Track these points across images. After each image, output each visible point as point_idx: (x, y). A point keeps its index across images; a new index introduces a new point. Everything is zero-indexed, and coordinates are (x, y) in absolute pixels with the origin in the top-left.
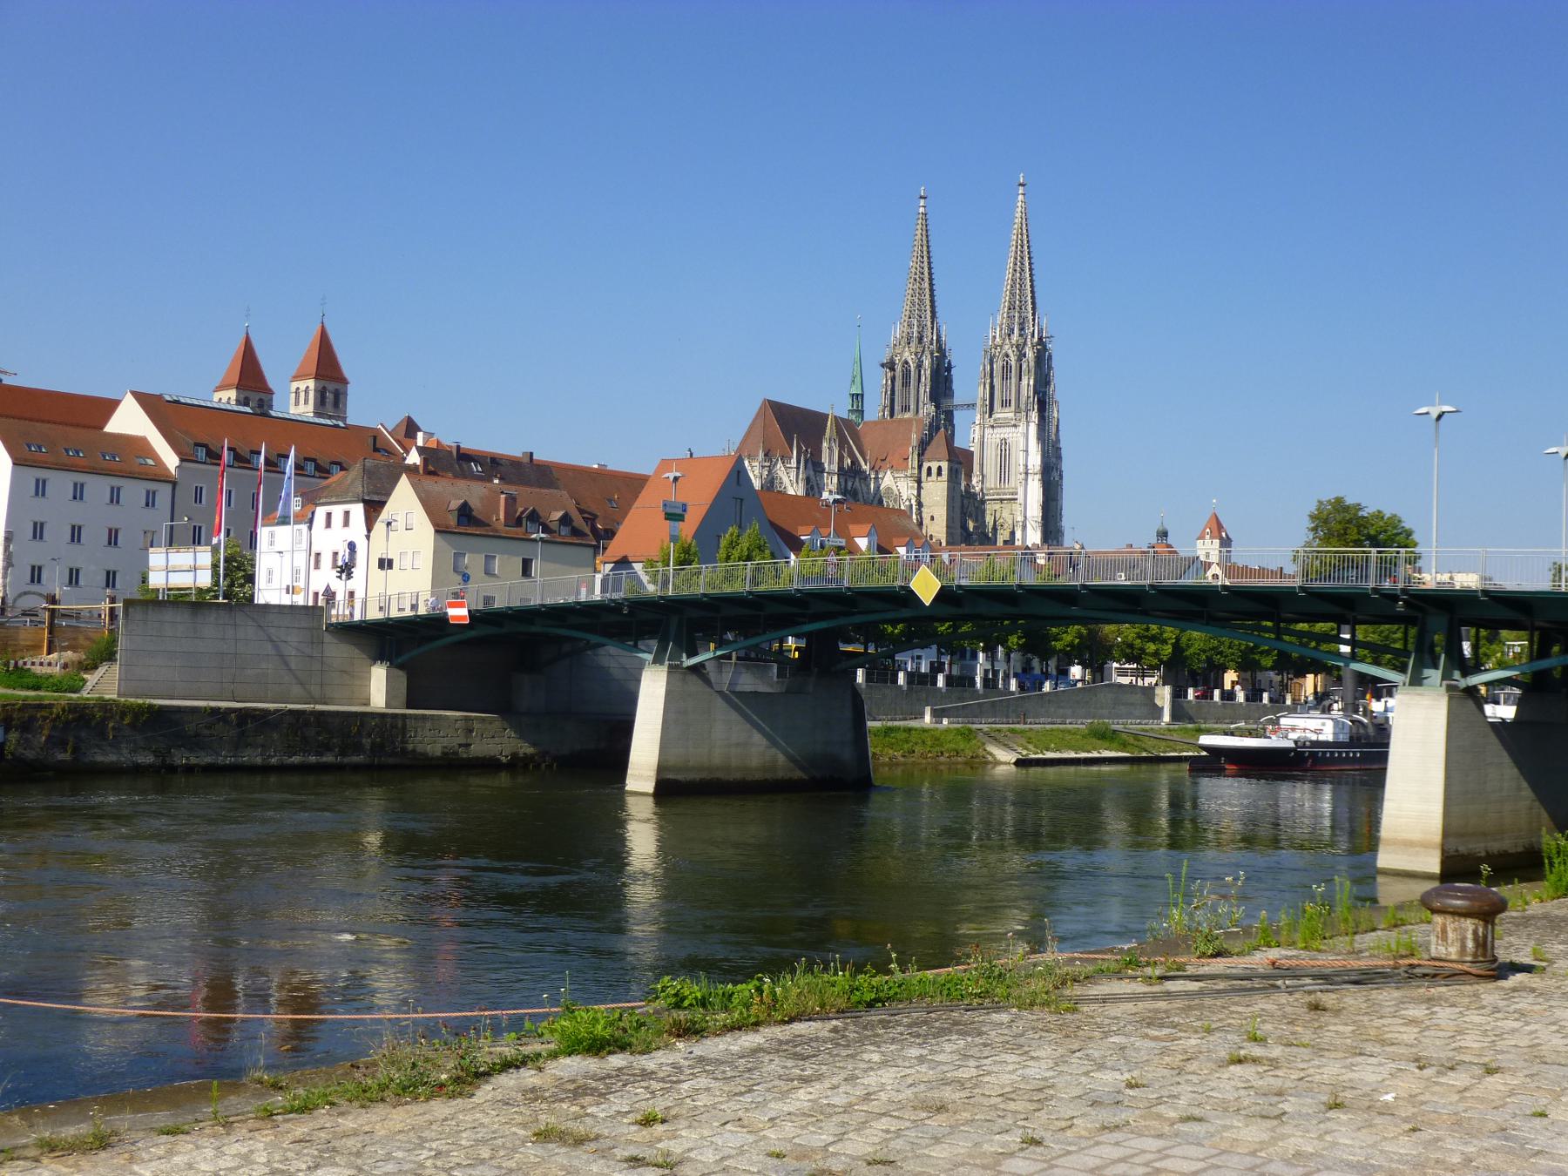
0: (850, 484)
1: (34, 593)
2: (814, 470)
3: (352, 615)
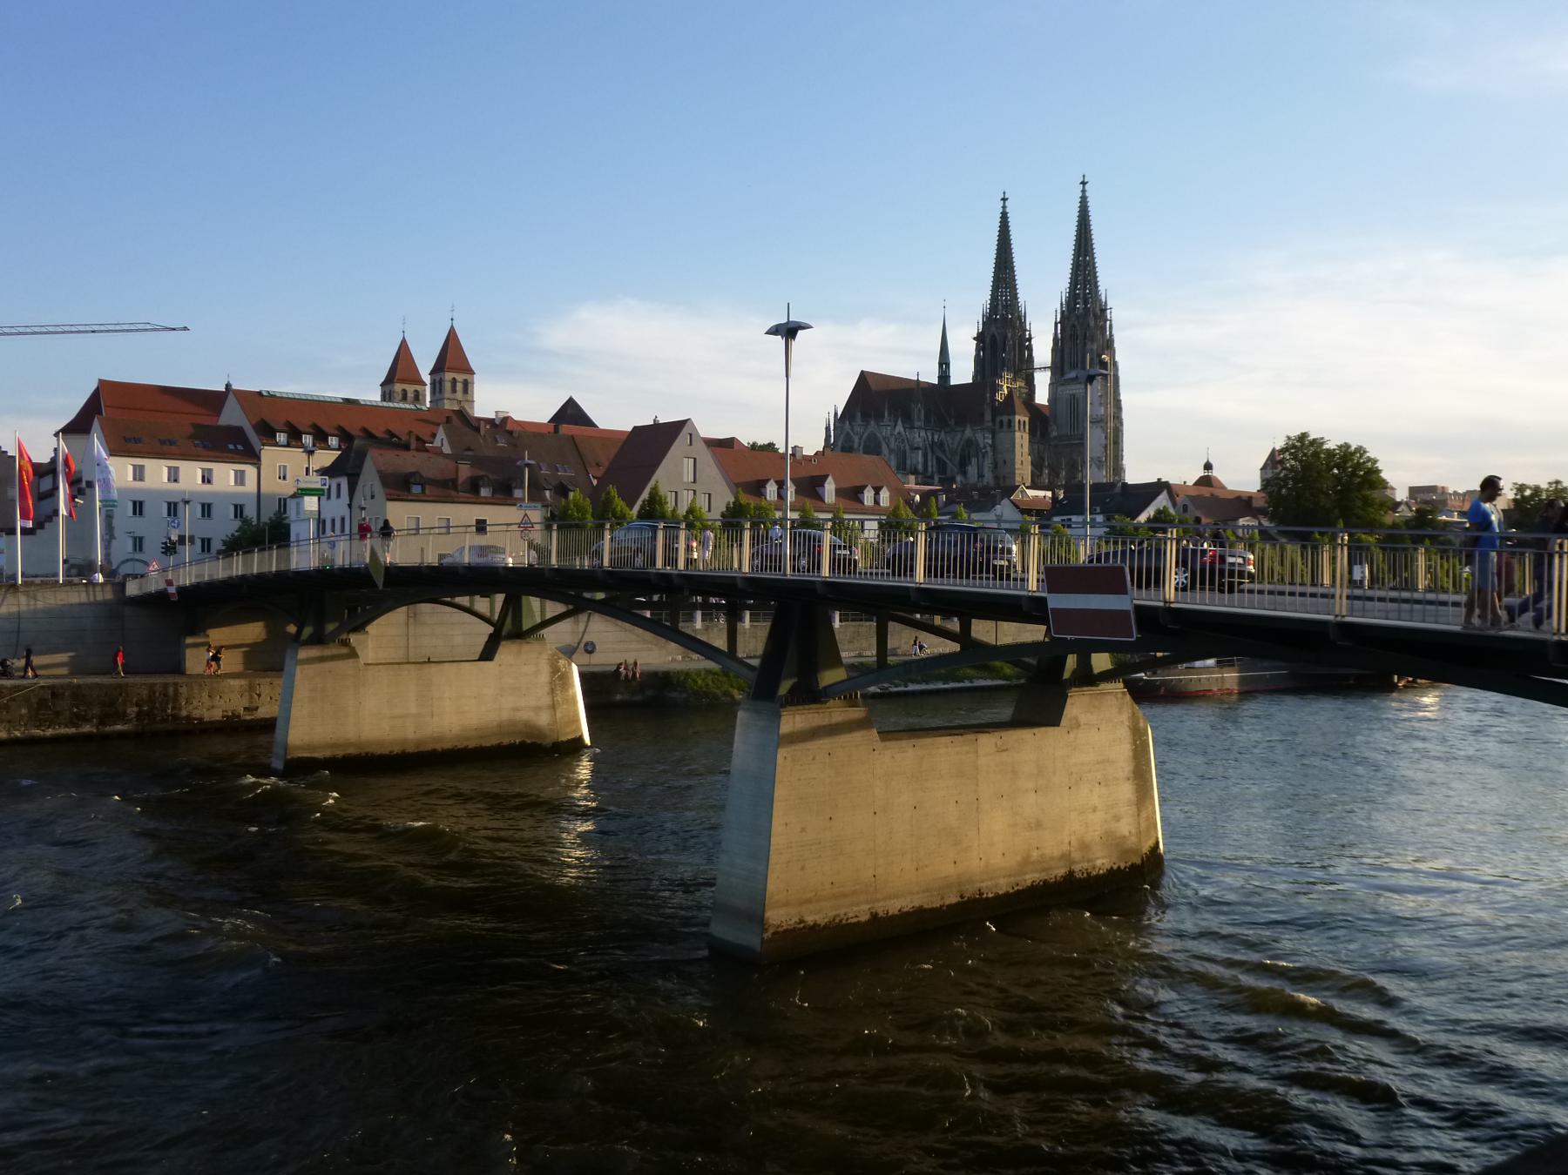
0: (936, 437)
1: (137, 560)
2: (903, 426)
3: (89, 599)
